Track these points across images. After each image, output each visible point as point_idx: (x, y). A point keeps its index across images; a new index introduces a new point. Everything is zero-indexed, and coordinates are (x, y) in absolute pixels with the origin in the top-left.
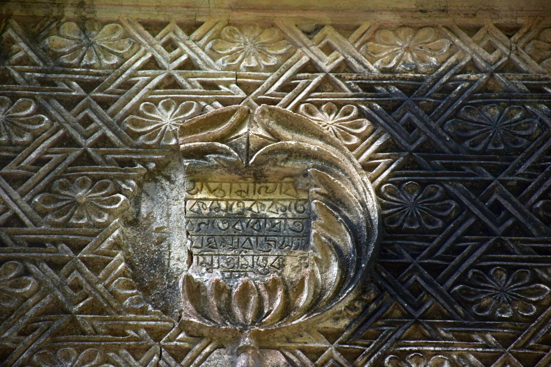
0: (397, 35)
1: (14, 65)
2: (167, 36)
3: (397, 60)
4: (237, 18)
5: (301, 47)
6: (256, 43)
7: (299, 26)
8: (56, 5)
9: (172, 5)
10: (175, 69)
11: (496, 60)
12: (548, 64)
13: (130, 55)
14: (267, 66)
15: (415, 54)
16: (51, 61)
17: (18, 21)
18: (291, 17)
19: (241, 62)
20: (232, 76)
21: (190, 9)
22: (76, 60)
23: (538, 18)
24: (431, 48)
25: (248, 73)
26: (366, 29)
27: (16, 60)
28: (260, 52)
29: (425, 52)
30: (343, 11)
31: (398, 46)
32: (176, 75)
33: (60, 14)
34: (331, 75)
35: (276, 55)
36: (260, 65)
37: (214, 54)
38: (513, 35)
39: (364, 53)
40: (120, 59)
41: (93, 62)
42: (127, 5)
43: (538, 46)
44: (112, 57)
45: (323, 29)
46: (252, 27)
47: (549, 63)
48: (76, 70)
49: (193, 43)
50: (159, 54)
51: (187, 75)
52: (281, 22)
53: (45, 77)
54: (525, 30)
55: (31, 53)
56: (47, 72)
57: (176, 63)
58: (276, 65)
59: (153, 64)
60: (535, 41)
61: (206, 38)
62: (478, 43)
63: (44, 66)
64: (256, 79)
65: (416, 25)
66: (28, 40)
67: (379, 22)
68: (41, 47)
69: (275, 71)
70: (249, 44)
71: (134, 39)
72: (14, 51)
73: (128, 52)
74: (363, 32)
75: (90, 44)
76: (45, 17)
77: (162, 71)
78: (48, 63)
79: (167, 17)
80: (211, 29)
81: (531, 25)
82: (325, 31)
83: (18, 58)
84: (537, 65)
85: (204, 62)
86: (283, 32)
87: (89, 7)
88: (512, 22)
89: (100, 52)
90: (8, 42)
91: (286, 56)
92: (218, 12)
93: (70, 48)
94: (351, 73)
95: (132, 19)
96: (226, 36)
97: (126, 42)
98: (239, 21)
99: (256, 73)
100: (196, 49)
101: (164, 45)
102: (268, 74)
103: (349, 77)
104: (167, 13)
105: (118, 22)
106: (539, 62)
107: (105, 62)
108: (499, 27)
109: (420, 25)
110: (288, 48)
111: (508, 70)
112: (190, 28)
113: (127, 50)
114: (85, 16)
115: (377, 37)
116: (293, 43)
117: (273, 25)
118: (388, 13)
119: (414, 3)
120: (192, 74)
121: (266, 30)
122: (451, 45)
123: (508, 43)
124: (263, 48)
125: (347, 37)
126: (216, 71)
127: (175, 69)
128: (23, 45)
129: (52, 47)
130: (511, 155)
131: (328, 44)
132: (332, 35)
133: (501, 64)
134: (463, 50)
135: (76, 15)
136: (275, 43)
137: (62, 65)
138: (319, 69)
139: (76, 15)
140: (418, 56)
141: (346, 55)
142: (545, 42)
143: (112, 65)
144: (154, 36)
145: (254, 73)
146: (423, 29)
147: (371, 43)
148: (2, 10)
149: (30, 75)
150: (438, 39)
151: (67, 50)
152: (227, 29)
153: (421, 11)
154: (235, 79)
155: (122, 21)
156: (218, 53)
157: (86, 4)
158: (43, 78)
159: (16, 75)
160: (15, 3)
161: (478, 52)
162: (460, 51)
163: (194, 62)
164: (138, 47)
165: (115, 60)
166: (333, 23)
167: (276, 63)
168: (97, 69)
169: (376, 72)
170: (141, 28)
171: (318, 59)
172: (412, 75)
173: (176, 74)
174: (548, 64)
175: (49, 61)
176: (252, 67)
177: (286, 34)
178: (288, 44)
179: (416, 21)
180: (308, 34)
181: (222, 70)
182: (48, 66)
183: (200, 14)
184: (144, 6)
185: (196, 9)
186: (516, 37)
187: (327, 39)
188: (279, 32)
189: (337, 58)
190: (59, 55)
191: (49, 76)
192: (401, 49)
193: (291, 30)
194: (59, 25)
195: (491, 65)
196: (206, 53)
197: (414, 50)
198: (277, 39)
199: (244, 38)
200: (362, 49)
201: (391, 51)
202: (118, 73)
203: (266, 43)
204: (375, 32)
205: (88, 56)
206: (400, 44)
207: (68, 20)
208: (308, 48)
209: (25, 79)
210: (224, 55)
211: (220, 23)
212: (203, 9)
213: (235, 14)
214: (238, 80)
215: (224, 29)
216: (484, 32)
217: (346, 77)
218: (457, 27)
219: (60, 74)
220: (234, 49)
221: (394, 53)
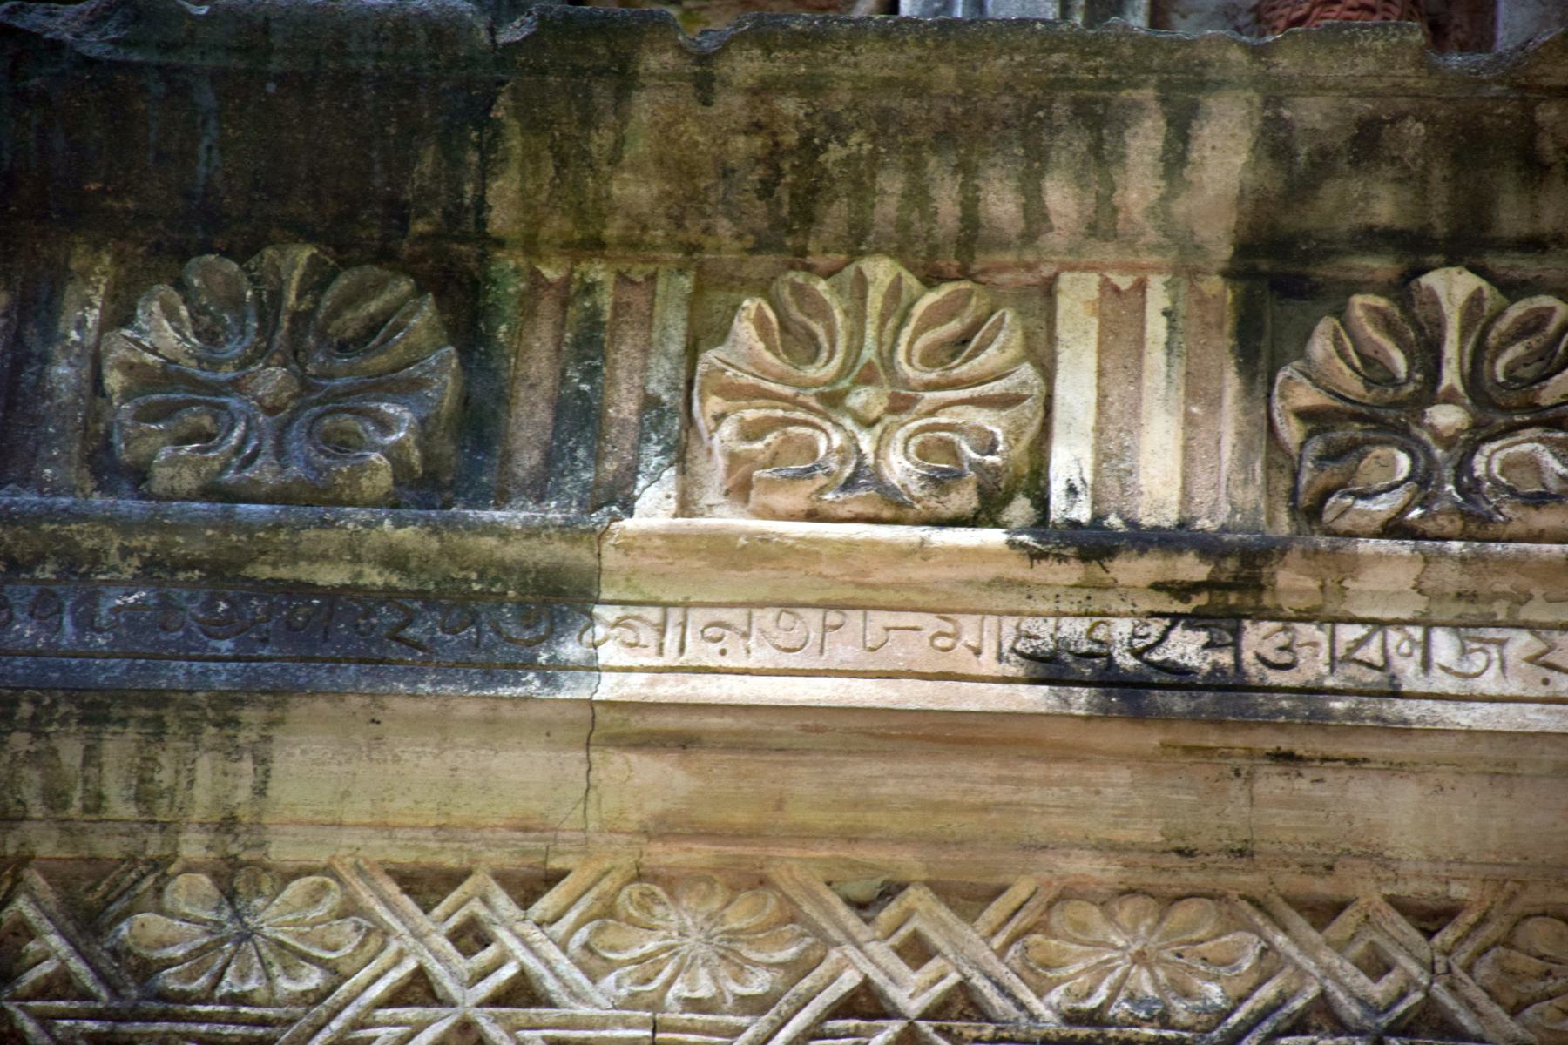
0: (1110, 918)
1: (28, 999)
2: (464, 911)
3: (1111, 987)
4: (665, 860)
5: (838, 944)
6: (715, 930)
7: (835, 885)
8: (157, 828)
9: (483, 823)
10: (479, 1005)
11: (1390, 999)
12: (1539, 1020)
13: (356, 965)
14: (743, 997)
15: (1160, 973)
16: (132, 984)
17: (48, 875)
18: (814, 859)
19: (669, 984)
20: (642, 1025)
21: (532, 835)
22: (203, 981)
23: (1508, 885)
24: (1209, 956)
25: (687, 1016)
26: (1024, 896)
27: (34, 984)
28: (723, 957)
29: (1189, 967)
30: (960, 844)
31: (1117, 949)
32: (483, 1022)
33: (167, 852)
34: (925, 1027)
35: (769, 966)
36: (722, 993)
37: (593, 962)
38: (1439, 930)
39: (1017, 964)
40: (328, 975)
41: (251, 985)
42: (356, 825)
43: (1507, 964)
44: (305, 971)
45: (902, 895)
46: (703, 887)
47: (1541, 1014)
48: (200, 1008)
49: (537, 930)
50: (439, 960)
51: (514, 1020)
52: (785, 874)
53: (111, 1033)
54: (1472, 918)
55: (77, 965)
56: (119, 1017)
57: (485, 988)
58: (767, 993)
59: (419, 989)
60: (1501, 949)
61: (572, 916)
62: (1340, 948)
63: (111, 1001)
64: (709, 1033)
65: (1164, 889)
66: (70, 926)
67: (1061, 878)
68: (107, 945)
69: (763, 1011)
70: (693, 931)
71: (369, 919)
72: (30, 959)
73: (351, 955)
74: (1015, 904)
75: (246, 935)
76: (123, 861)
77: (444, 1011)
78: (123, 992)
79: (465, 856)
80: (588, 890)
81: (1488, 903)
82: (909, 899)
83: (38, 979)
84: (1507, 1018)
85: (566, 985)
86: (790, 901)
87: (248, 831)
88: (1435, 894)
89: (270, 957)
90: (16, 934)
91: (798, 968)
92: (609, 843)
93: (190, 946)
94: (979, 1020)
95: (367, 862)
96: (631, 910)
97: (348, 925)
98: (668, 867)
99: (710, 1017)
100: (544, 947)
101: (455, 936)
102: (745, 1020)
103: (975, 1034)
104: (467, 846)
105: (327, 870)
106: (1515, 1011)
107: (285, 985)
108: (1399, 905)
109: (1178, 890)
110: (803, 945)
111: (1426, 1028)
112: (529, 887)
113: (348, 949)
114: (235, 857)
115: (1055, 919)
116: (818, 932)
117: (763, 882)
118: (1087, 853)
119: (1159, 828)
120: (530, 1020)
121: (745, 895)
122: (1264, 951)
123: (1425, 953)
124: (733, 945)
125: (970, 917)
126: (596, 1012)
127: (479, 1005)
128: (55, 941)
129: (138, 944)
130: (260, 659)
131: (916, 936)
132: (929, 912)
133: (1406, 1013)
134: (1298, 967)
135: (212, 854)
136: (768, 931)
137: (162, 996)
138: (888, 1008)
139: (212, 854)
140: (1171, 980)
141: (966, 970)
142: (1529, 954)
143: (304, 993)
144: (427, 909)
145: (704, 1017)
146: (1185, 902)
147: (1037, 938)
148: (4, 844)
149: (69, 1028)
150: (1228, 932)
151: (180, 953)
152: (635, 889)
153: (1180, 852)
154: (649, 1033)
155: (339, 868)
156: (605, 959)
157: (240, 823)
158: (106, 1034)
159: (30, 1027)
160: (43, 824)
161: (1340, 973)
162: (1289, 970)
163: (537, 985)
164: (380, 940)
165: (313, 979)
166: (933, 877)
167: (767, 987)
168: (259, 1006)
169: (1051, 1023)
170: (392, 889)
171: (886, 979)
172: (1152, 1032)
173: (484, 1020)
174: (1539, 1020)
175: (125, 986)
176: (699, 1000)
177: (799, 906)
178: (804, 935)
179: (1163, 880)
180: (860, 906)
181: (615, 1008)
182: (122, 998)
183: (561, 847)
184: (401, 827)
185: (547, 834)
186: (1448, 935)
187: (915, 924)
188: (779, 900)
189: (942, 977)
190: (155, 967)
191: (124, 1027)
192: (1122, 958)
193: (820, 902)
194: (161, 882)
195: (1378, 1014)
196: (571, 958)
197: (1160, 961)
198: (773, 920)
199: (680, 918)
200: (1011, 953)
201: (1093, 961)
202: (318, 1015)
203: (741, 931)
204: (1050, 905)
205: (239, 969)
206: (1121, 943)
207: (189, 869)
208: (859, 947)
209: (53, 1037)
210: (622, 964)
211: (614, 874)
212: (567, 835)
213: (657, 847)
214: (659, 1036)
215: (626, 891)
216: (1358, 916)
217: (966, 1033)
218: (1279, 900)
219: (155, 1021)
220: (650, 946)
221: (1104, 968)
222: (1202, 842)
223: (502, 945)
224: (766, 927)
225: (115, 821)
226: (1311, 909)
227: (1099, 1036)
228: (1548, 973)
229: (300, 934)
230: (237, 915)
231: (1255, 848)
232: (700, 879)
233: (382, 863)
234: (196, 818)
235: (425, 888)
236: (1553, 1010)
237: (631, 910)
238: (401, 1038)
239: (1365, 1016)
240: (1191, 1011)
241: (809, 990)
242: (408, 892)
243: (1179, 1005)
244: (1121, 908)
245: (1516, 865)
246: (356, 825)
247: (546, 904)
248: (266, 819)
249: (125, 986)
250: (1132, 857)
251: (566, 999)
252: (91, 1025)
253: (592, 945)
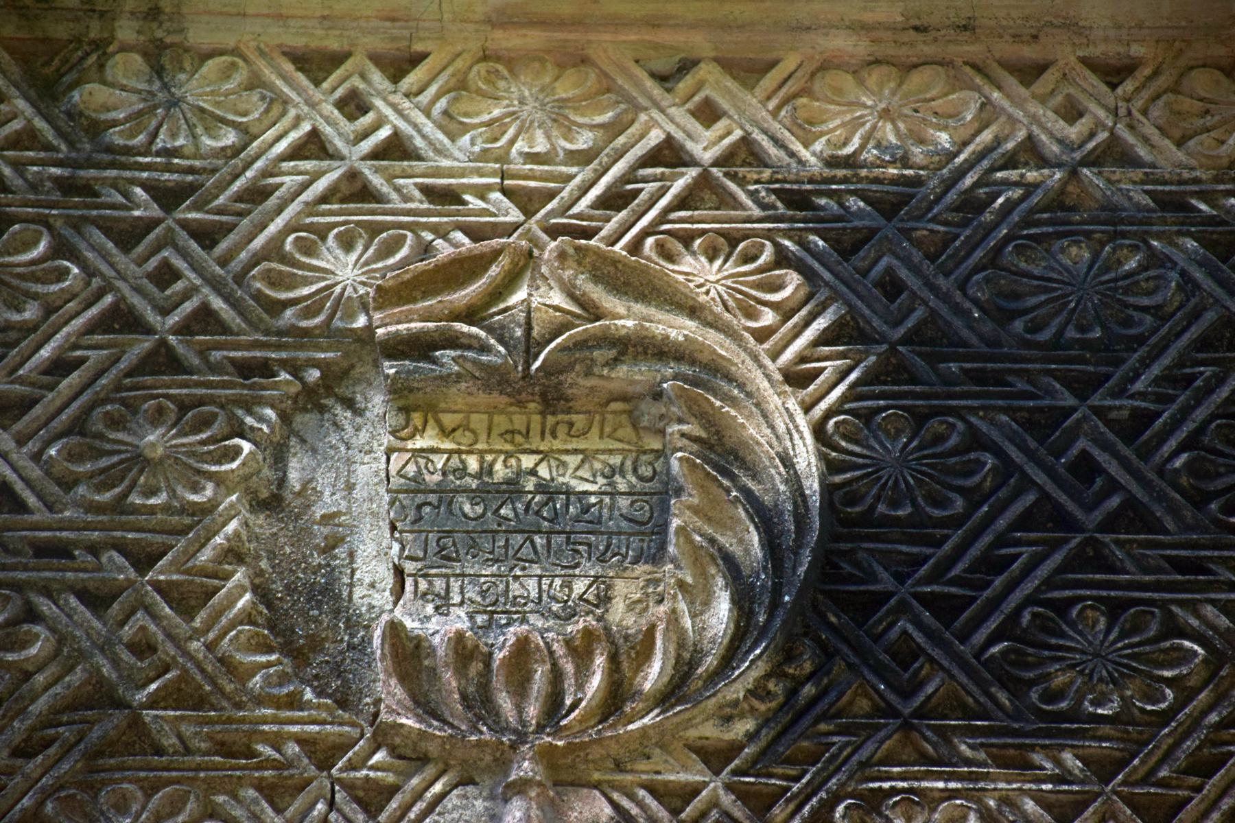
0: (861, 83)
2: (347, 85)
4: (505, 44)
5: (646, 109)
6: (547, 100)
7: (642, 63)
8: (96, 16)
10: (363, 159)
11: (1082, 138)
12: (1199, 148)
13: (263, 127)
15: (901, 125)
16: (85, 140)
19: (512, 142)
20: (493, 174)
21: (398, 24)
22: (141, 138)
23: (1177, 43)
25: (528, 167)
28: (555, 120)
29: (924, 119)
30: (741, 27)
31: (865, 106)
32: (367, 172)
33: (106, 35)
35: (592, 127)
36: (555, 149)
37: (452, 125)
38: (1121, 82)
39: (787, 122)
40: (241, 135)
41: (180, 142)
42: (257, 16)
44: (223, 132)
45: (695, 69)
46: (537, 65)
48: (141, 159)
49: (405, 100)
50: (328, 124)
51: (391, 171)
54: (1147, 71)
55: (39, 123)
56: (76, 165)
57: (367, 145)
58: (590, 149)
59: (314, 146)
60: (1170, 95)
61: (433, 89)
62: (1042, 100)
63: (69, 152)
64: (546, 180)
65: (904, 59)
66: (32, 93)
68: (63, 108)
69: (589, 162)
71: (272, 91)
73: (259, 119)
74: (785, 75)
75: (174, 103)
76: (71, 42)
77: (335, 164)
78: (78, 146)
79: (346, 43)
80: (444, 68)
81: (1160, 59)
82: (701, 73)
83: (10, 134)
84: (1174, 149)
86: (606, 75)
87: (170, 20)
88: (1119, 54)
89: (194, 120)
91: (615, 129)
92: (461, 31)
93: (129, 111)
94: (758, 166)
96: (480, 84)
97: (255, 97)
98: (508, 50)
99: (546, 168)
100: (412, 114)
101: (341, 105)
102: (574, 170)
103: (755, 177)
104: (347, 33)
105: (236, 52)
106: (1179, 144)
107: (208, 142)
108: (1088, 63)
109: (915, 60)
110: (618, 110)
111: (1111, 159)
112: (398, 66)
113: (256, 115)
114: (161, 40)
115: (817, 86)
116: (630, 100)
117: (585, 61)
118: (842, 32)
120: (404, 170)
122: (983, 105)
125: (750, 87)
126: (456, 164)
127: (363, 159)
128: (21, 104)
129: (87, 108)
131: (707, 102)
133: (1095, 148)
134: (1010, 116)
136: (590, 100)
137: (110, 149)
138: (687, 158)
139: (142, 38)
140: (910, 130)
141: (748, 127)
142: (1192, 98)
143: (223, 149)
144: (317, 83)
145: (541, 167)
146: (921, 68)
147: (804, 100)
149: (38, 173)
150: (953, 91)
151: (121, 116)
152: (482, 67)
153: (916, 29)
154: (498, 180)
155: (245, 50)
156: (461, 123)
157: (163, 12)
158: (68, 178)
161: (1043, 120)
162: (1003, 119)
163: (407, 144)
165: (230, 138)
166: (720, 55)
167: (591, 143)
168: (188, 158)
170: (288, 67)
175: (80, 141)
176: (537, 154)
177: (613, 80)
178: (618, 102)
179: (903, 51)
180: (664, 79)
181: (470, 161)
182: (78, 150)
183: (421, 34)
184: (293, 17)
186: (1128, 86)
188: (598, 76)
189: (729, 133)
190: (102, 126)
191: (82, 173)
192: (871, 114)
194: (103, 59)
195: (1073, 150)
196: (434, 122)
198: (593, 90)
199: (520, 90)
200: (783, 113)
201: (848, 117)
202: (236, 166)
204: (813, 75)
205: (169, 129)
206: (870, 103)
207: (124, 49)
208: (662, 111)
209: (26, 180)
210: (475, 126)
211: (465, 55)
212: (427, 24)
213: (499, 34)
214: (506, 182)
215: (475, 69)
217: (749, 176)
218: (995, 65)
219: (106, 168)
220: (496, 112)
221: (857, 123)
222: (934, 20)
223: (379, 111)
224: (588, 97)
225: (63, 9)
226: (1020, 70)
227: (854, 176)
228: (1207, 112)
229: (217, 103)
230: (165, 87)
231: (977, 23)
232: (534, 59)
233: (280, 46)
234: (127, 8)
235: (314, 67)
236: (1210, 140)
237: (480, 84)
238: (302, 184)
239: (1063, 153)
240: (927, 154)
241: (624, 145)
242: (299, 69)
243: (917, 150)
244: (870, 75)
245: (1184, 28)
246: (257, 16)
247: (411, 79)
248: (185, 10)
249: (80, 141)
250: (879, 34)
251: (431, 154)
252: (54, 171)
253: (450, 111)
